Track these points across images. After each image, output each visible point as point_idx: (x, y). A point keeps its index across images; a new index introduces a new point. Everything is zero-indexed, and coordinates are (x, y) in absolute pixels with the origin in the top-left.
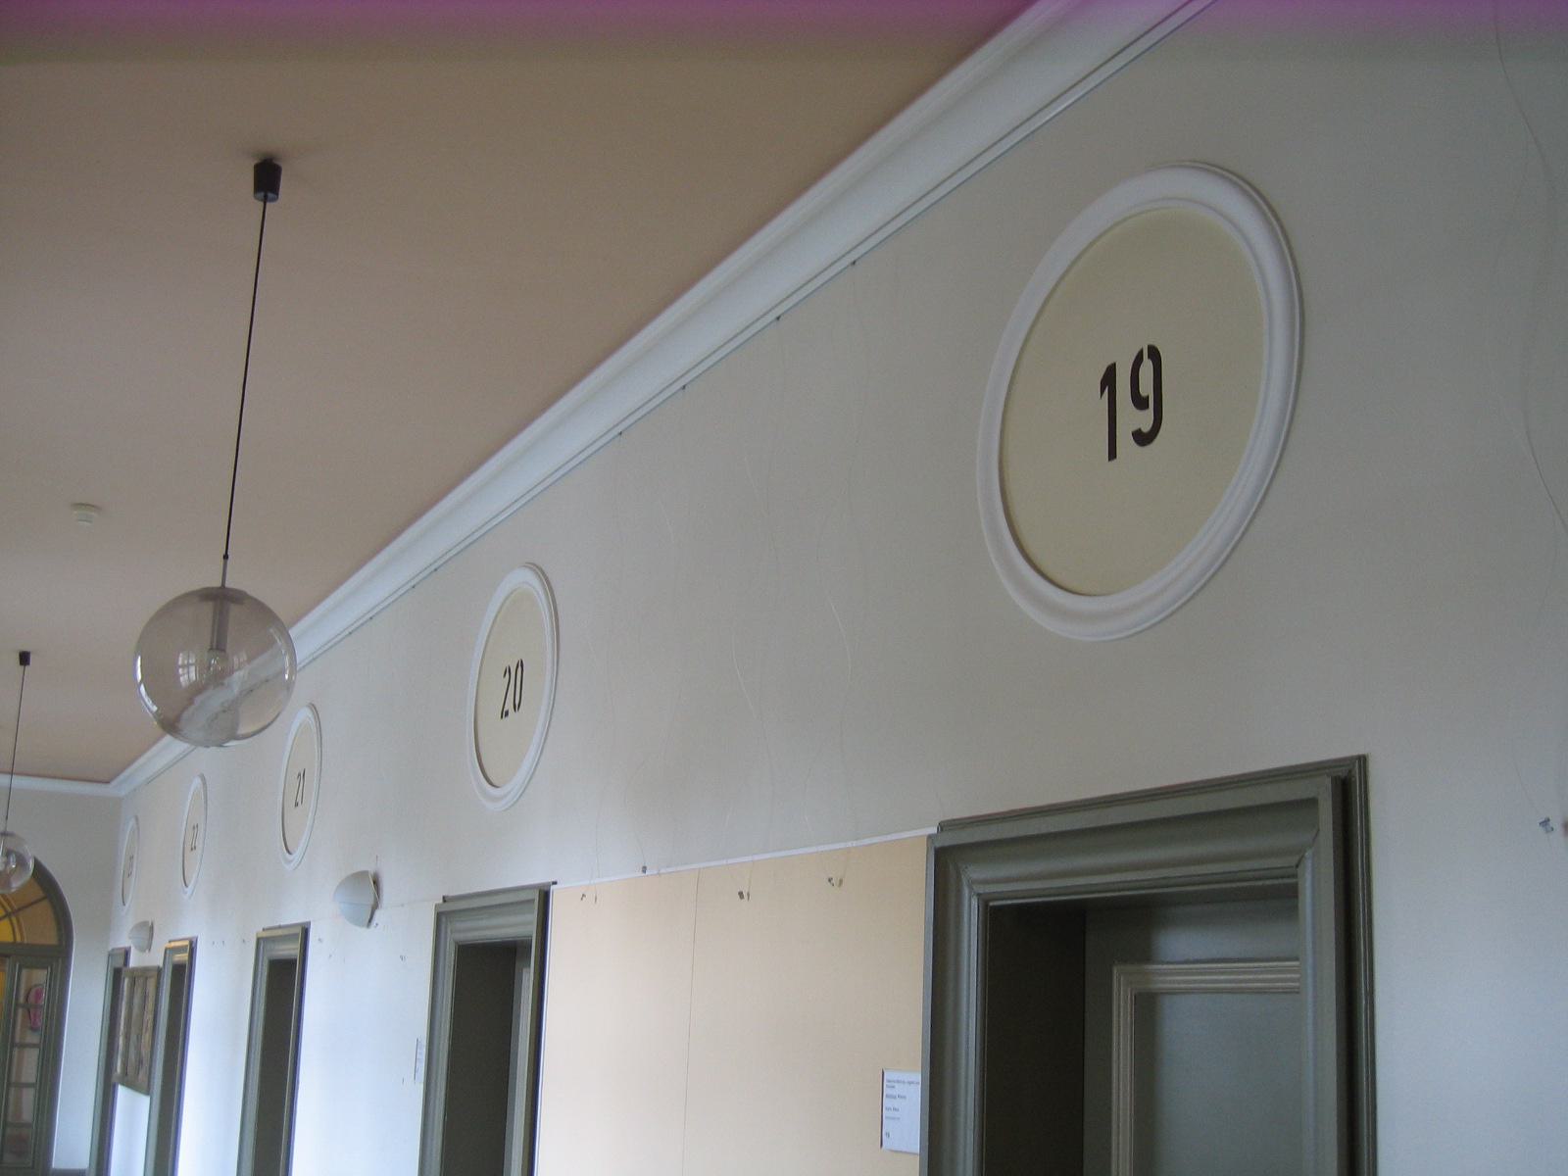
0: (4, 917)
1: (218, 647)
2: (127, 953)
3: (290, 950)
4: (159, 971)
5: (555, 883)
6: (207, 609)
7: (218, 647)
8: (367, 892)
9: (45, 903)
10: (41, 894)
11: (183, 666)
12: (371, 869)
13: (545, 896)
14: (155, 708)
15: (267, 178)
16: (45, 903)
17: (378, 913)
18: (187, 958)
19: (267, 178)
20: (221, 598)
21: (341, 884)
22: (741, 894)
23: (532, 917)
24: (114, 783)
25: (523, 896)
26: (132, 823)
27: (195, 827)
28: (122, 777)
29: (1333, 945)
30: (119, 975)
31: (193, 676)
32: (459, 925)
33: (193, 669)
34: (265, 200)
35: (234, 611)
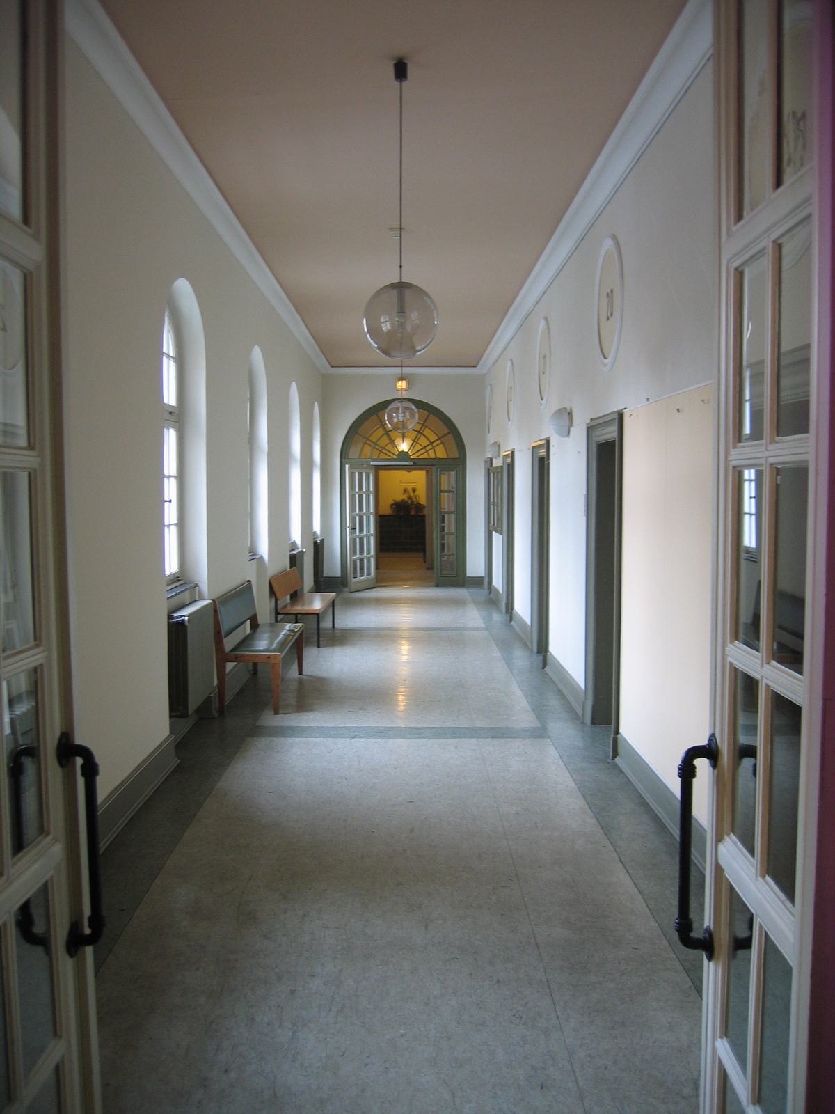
0: (434, 450)
1: (402, 311)
2: (491, 460)
3: (610, 433)
4: (502, 467)
5: (625, 409)
6: (395, 292)
7: (402, 311)
8: (565, 416)
9: (450, 436)
10: (447, 431)
11: (383, 322)
12: (567, 406)
13: (621, 416)
14: (376, 346)
15: (401, 70)
16: (450, 436)
17: (572, 429)
18: (544, 453)
19: (401, 70)
20: (401, 287)
21: (553, 414)
22: (678, 410)
23: (615, 428)
24: (479, 366)
25: (609, 418)
26: (489, 388)
27: (511, 388)
28: (481, 362)
29: (483, 509)
30: (490, 470)
31: (388, 326)
32: (598, 433)
33: (388, 323)
34: (401, 81)
35: (407, 292)
